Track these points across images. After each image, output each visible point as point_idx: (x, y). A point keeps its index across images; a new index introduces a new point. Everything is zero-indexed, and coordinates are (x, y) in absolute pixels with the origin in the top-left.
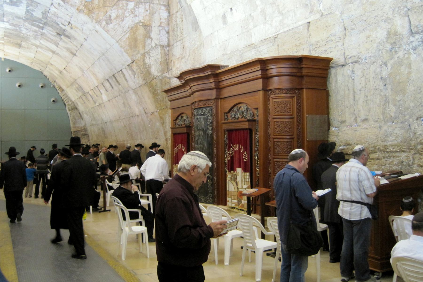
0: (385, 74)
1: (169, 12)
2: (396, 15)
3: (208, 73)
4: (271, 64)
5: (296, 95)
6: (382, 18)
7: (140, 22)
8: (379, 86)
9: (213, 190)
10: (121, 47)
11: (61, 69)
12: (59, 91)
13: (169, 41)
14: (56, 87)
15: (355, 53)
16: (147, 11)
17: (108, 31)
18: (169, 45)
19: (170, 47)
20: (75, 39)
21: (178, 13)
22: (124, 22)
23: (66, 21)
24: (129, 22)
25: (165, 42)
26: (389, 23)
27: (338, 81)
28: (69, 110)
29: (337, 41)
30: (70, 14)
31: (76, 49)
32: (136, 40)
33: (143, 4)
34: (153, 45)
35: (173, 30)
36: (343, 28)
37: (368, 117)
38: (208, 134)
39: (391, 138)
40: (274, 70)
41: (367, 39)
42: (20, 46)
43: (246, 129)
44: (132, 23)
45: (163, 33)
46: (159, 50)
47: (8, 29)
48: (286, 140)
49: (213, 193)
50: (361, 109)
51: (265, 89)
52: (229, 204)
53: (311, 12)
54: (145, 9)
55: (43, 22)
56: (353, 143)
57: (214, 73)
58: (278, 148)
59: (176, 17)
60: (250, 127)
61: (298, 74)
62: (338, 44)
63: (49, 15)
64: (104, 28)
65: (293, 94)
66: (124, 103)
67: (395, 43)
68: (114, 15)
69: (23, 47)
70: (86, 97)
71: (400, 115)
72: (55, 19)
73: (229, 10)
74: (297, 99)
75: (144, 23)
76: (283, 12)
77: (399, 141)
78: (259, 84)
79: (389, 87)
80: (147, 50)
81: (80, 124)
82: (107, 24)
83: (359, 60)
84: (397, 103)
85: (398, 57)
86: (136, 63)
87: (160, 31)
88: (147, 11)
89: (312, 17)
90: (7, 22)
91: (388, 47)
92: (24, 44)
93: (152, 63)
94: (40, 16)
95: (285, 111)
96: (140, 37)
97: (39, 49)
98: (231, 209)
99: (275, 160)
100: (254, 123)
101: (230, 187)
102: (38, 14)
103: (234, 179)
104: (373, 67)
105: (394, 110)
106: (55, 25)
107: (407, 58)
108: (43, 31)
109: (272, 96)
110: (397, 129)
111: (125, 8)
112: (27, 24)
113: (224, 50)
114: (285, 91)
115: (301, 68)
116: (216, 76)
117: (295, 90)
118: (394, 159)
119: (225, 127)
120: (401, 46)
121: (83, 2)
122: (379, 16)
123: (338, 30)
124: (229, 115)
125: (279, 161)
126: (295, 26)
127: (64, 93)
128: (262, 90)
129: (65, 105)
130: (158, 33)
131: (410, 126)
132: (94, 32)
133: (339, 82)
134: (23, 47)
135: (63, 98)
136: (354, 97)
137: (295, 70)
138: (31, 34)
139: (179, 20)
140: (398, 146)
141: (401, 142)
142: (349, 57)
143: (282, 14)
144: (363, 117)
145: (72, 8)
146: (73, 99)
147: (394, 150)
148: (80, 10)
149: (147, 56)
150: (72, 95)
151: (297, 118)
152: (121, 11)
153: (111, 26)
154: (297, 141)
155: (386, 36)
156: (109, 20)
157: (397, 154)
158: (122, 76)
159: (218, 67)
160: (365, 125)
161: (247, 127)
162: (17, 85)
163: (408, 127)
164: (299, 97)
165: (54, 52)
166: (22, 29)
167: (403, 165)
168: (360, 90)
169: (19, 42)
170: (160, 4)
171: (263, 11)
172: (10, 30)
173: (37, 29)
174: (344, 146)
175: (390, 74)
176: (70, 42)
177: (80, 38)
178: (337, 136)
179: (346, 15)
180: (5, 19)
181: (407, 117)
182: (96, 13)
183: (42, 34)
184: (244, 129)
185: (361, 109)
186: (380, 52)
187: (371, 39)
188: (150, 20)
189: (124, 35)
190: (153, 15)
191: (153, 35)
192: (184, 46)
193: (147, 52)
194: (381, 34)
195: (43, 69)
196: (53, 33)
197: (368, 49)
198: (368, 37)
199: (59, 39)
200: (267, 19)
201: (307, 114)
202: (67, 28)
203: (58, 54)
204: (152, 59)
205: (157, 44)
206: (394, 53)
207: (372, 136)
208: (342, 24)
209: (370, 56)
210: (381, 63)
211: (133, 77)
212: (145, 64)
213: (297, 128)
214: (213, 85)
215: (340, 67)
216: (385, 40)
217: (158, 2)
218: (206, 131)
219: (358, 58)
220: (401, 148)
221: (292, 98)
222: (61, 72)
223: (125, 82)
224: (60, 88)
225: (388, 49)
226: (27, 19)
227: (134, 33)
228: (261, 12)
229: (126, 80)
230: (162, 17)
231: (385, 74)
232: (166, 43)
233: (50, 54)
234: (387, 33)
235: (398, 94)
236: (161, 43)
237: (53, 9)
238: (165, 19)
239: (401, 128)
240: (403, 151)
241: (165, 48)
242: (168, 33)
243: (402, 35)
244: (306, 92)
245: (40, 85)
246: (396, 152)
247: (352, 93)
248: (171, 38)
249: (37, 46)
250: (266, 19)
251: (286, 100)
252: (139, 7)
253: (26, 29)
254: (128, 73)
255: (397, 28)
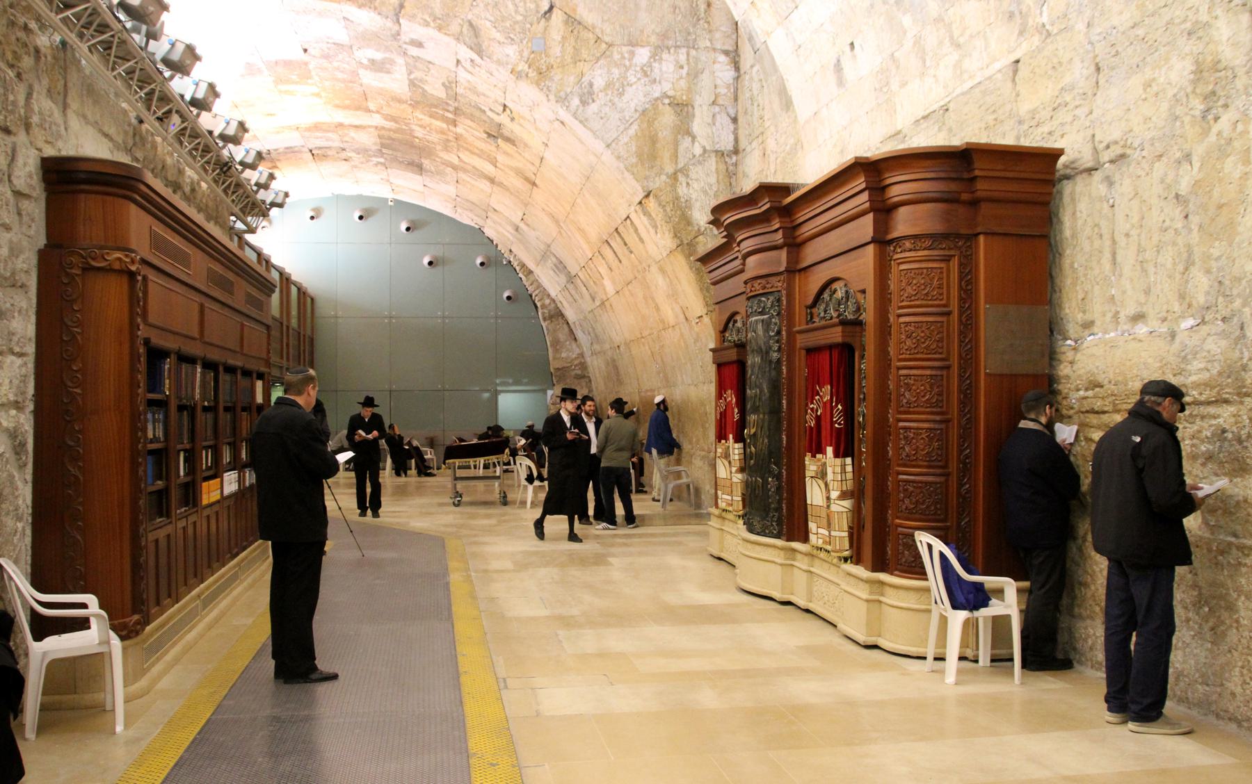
0: (1184, 187)
1: (737, 69)
2: (1219, 12)
3: (764, 205)
4: (892, 170)
5: (958, 253)
6: (1183, 26)
7: (665, 96)
8: (1172, 220)
9: (780, 502)
10: (618, 158)
11: (516, 220)
12: (521, 275)
13: (736, 140)
14: (515, 264)
15: (1116, 135)
16: (682, 67)
17: (586, 120)
18: (736, 151)
19: (740, 156)
20: (526, 145)
21: (755, 69)
22: (625, 98)
23: (496, 101)
24: (636, 97)
25: (727, 143)
26: (1200, 38)
27: (1078, 214)
28: (545, 319)
29: (1077, 103)
30: (500, 85)
31: (533, 169)
32: (654, 140)
33: (672, 50)
34: (698, 150)
35: (746, 113)
36: (1093, 68)
37: (1144, 310)
38: (771, 362)
39: (1197, 365)
40: (900, 187)
41: (1145, 90)
42: (419, 168)
43: (837, 345)
44: (643, 99)
45: (723, 120)
46: (712, 163)
47: (383, 128)
48: (928, 372)
49: (779, 509)
50: (1128, 287)
51: (882, 241)
52: (812, 538)
53: (1021, 33)
54: (677, 62)
55: (451, 109)
56: (1106, 382)
57: (777, 204)
58: (907, 394)
59: (751, 78)
60: (848, 340)
61: (965, 197)
62: (1077, 112)
63: (460, 90)
64: (575, 115)
65: (950, 249)
66: (645, 298)
67: (1213, 93)
68: (599, 82)
69: (427, 171)
70: (576, 288)
71: (1221, 299)
72: (474, 98)
73: (848, 48)
74: (960, 264)
75: (674, 98)
76: (961, 40)
77: (1215, 372)
78: (865, 228)
79: (1195, 220)
80: (680, 165)
81: (569, 353)
82: (584, 103)
83: (1128, 152)
84: (1214, 264)
85: (1219, 134)
86: (656, 196)
87: (714, 116)
88: (682, 67)
89: (1024, 44)
90: (378, 112)
91: (1198, 106)
92: (426, 163)
93: (694, 196)
94: (441, 94)
95: (927, 294)
96: (665, 134)
97: (462, 175)
98: (815, 552)
99: (901, 424)
100: (858, 329)
101: (814, 495)
102: (435, 89)
103: (822, 475)
104: (1160, 168)
105: (1206, 288)
106: (478, 114)
107: (1241, 134)
108: (459, 130)
109: (896, 257)
110: (1210, 339)
111: (627, 63)
112: (418, 114)
113: (842, 151)
114: (928, 243)
115: (973, 179)
116: (787, 212)
117: (953, 241)
118: (1205, 425)
119: (802, 341)
120: (1230, 101)
121: (526, 54)
122: (1177, 21)
123: (1078, 73)
124: (815, 310)
125: (910, 428)
126: (987, 73)
127: (531, 278)
128: (873, 241)
129: (536, 307)
130: (710, 121)
131: (1242, 328)
132: (557, 124)
133: (1083, 214)
134: (427, 171)
135: (530, 289)
136: (1114, 254)
137: (953, 187)
138: (434, 137)
139: (756, 86)
140: (1212, 388)
141: (1220, 374)
142: (1104, 144)
143: (958, 46)
144: (1131, 310)
145: (500, 69)
146: (553, 294)
147: (1203, 398)
148: (519, 73)
149: (681, 178)
150: (550, 282)
151: (960, 315)
152: (616, 71)
153: (593, 107)
154: (960, 376)
155: (1192, 76)
156: (587, 97)
157: (1212, 410)
158: (632, 230)
159: (785, 189)
160: (1142, 329)
161: (839, 340)
162: (426, 260)
163: (1238, 333)
164: (966, 257)
165: (492, 181)
166: (414, 127)
167: (1225, 439)
168: (1127, 235)
169: (416, 158)
170: (714, 50)
171: (918, 41)
172: (390, 130)
173: (444, 126)
174: (1087, 390)
175: (1197, 184)
176: (516, 155)
177: (535, 141)
178: (1071, 363)
179: (1099, 30)
180: (372, 106)
181: (1238, 303)
182: (556, 78)
183: (458, 138)
184: (831, 347)
185: (1128, 287)
186: (1178, 124)
187: (1155, 88)
188: (689, 90)
189: (626, 129)
190: (696, 76)
191: (697, 126)
192: (764, 149)
193: (681, 170)
194: (1178, 71)
195: (481, 222)
196: (476, 133)
197: (1147, 119)
198: (1147, 85)
199: (493, 148)
200: (928, 64)
201: (986, 302)
202: (504, 119)
203: (500, 185)
204: (695, 185)
205: (708, 148)
206: (1212, 122)
207: (1150, 360)
208: (1092, 55)
209: (1153, 139)
210: (1178, 155)
211: (652, 231)
212: (678, 198)
213: (961, 341)
214: (779, 238)
215: (1084, 175)
216: (1189, 90)
217: (708, 44)
218: (767, 353)
219: (1124, 146)
220: (1218, 393)
221: (947, 259)
222: (517, 229)
223: (641, 246)
224: (523, 266)
225: (1197, 113)
226: (417, 103)
227: (650, 123)
228: (915, 44)
229: (641, 240)
230: (719, 82)
231: (1184, 187)
232: (730, 147)
233: (484, 185)
234: (1194, 68)
235: (1217, 239)
236: (717, 147)
237: (463, 75)
238: (728, 87)
239: (1223, 334)
240: (1226, 401)
241: (727, 159)
242: (735, 120)
243: (1232, 69)
244: (986, 245)
245: (479, 261)
246: (1209, 403)
247: (1108, 243)
248: (740, 132)
249: (455, 168)
250: (924, 62)
251: (930, 265)
252: (661, 59)
253: (421, 126)
254: (640, 221)
255: (1220, 49)
